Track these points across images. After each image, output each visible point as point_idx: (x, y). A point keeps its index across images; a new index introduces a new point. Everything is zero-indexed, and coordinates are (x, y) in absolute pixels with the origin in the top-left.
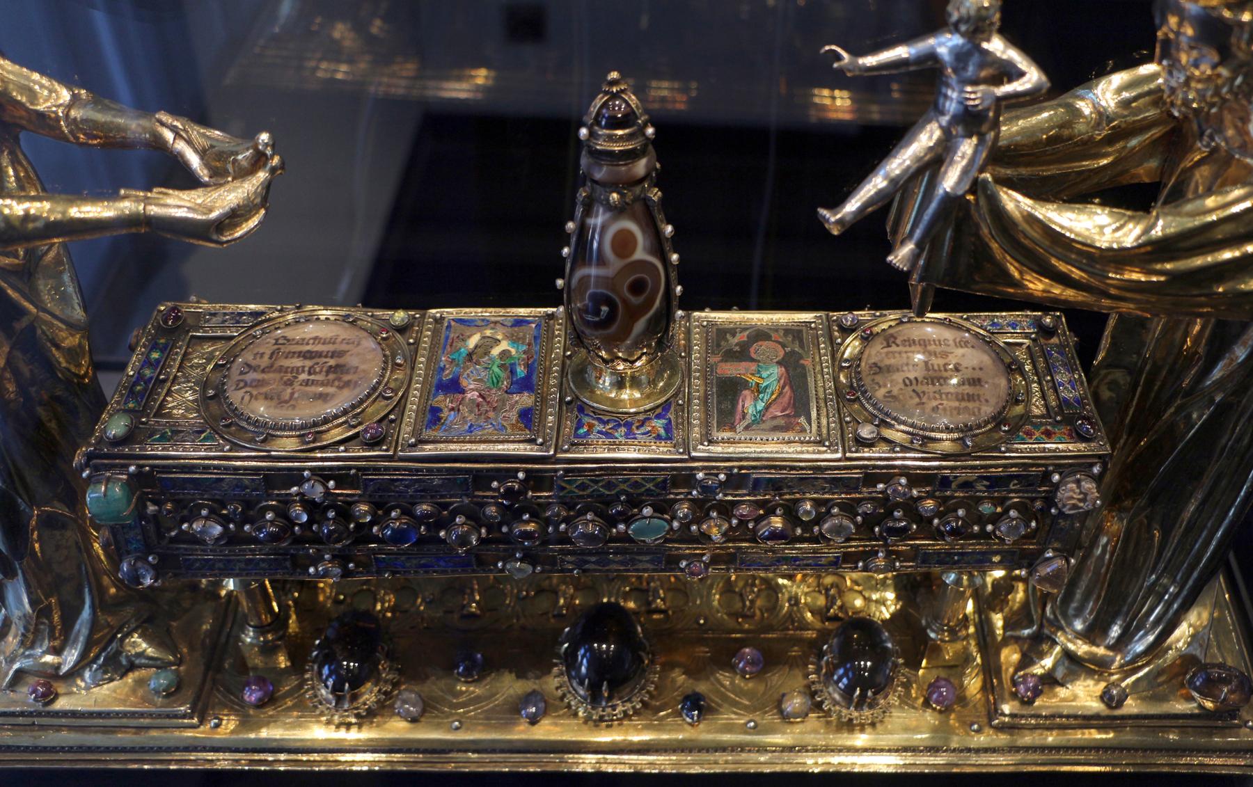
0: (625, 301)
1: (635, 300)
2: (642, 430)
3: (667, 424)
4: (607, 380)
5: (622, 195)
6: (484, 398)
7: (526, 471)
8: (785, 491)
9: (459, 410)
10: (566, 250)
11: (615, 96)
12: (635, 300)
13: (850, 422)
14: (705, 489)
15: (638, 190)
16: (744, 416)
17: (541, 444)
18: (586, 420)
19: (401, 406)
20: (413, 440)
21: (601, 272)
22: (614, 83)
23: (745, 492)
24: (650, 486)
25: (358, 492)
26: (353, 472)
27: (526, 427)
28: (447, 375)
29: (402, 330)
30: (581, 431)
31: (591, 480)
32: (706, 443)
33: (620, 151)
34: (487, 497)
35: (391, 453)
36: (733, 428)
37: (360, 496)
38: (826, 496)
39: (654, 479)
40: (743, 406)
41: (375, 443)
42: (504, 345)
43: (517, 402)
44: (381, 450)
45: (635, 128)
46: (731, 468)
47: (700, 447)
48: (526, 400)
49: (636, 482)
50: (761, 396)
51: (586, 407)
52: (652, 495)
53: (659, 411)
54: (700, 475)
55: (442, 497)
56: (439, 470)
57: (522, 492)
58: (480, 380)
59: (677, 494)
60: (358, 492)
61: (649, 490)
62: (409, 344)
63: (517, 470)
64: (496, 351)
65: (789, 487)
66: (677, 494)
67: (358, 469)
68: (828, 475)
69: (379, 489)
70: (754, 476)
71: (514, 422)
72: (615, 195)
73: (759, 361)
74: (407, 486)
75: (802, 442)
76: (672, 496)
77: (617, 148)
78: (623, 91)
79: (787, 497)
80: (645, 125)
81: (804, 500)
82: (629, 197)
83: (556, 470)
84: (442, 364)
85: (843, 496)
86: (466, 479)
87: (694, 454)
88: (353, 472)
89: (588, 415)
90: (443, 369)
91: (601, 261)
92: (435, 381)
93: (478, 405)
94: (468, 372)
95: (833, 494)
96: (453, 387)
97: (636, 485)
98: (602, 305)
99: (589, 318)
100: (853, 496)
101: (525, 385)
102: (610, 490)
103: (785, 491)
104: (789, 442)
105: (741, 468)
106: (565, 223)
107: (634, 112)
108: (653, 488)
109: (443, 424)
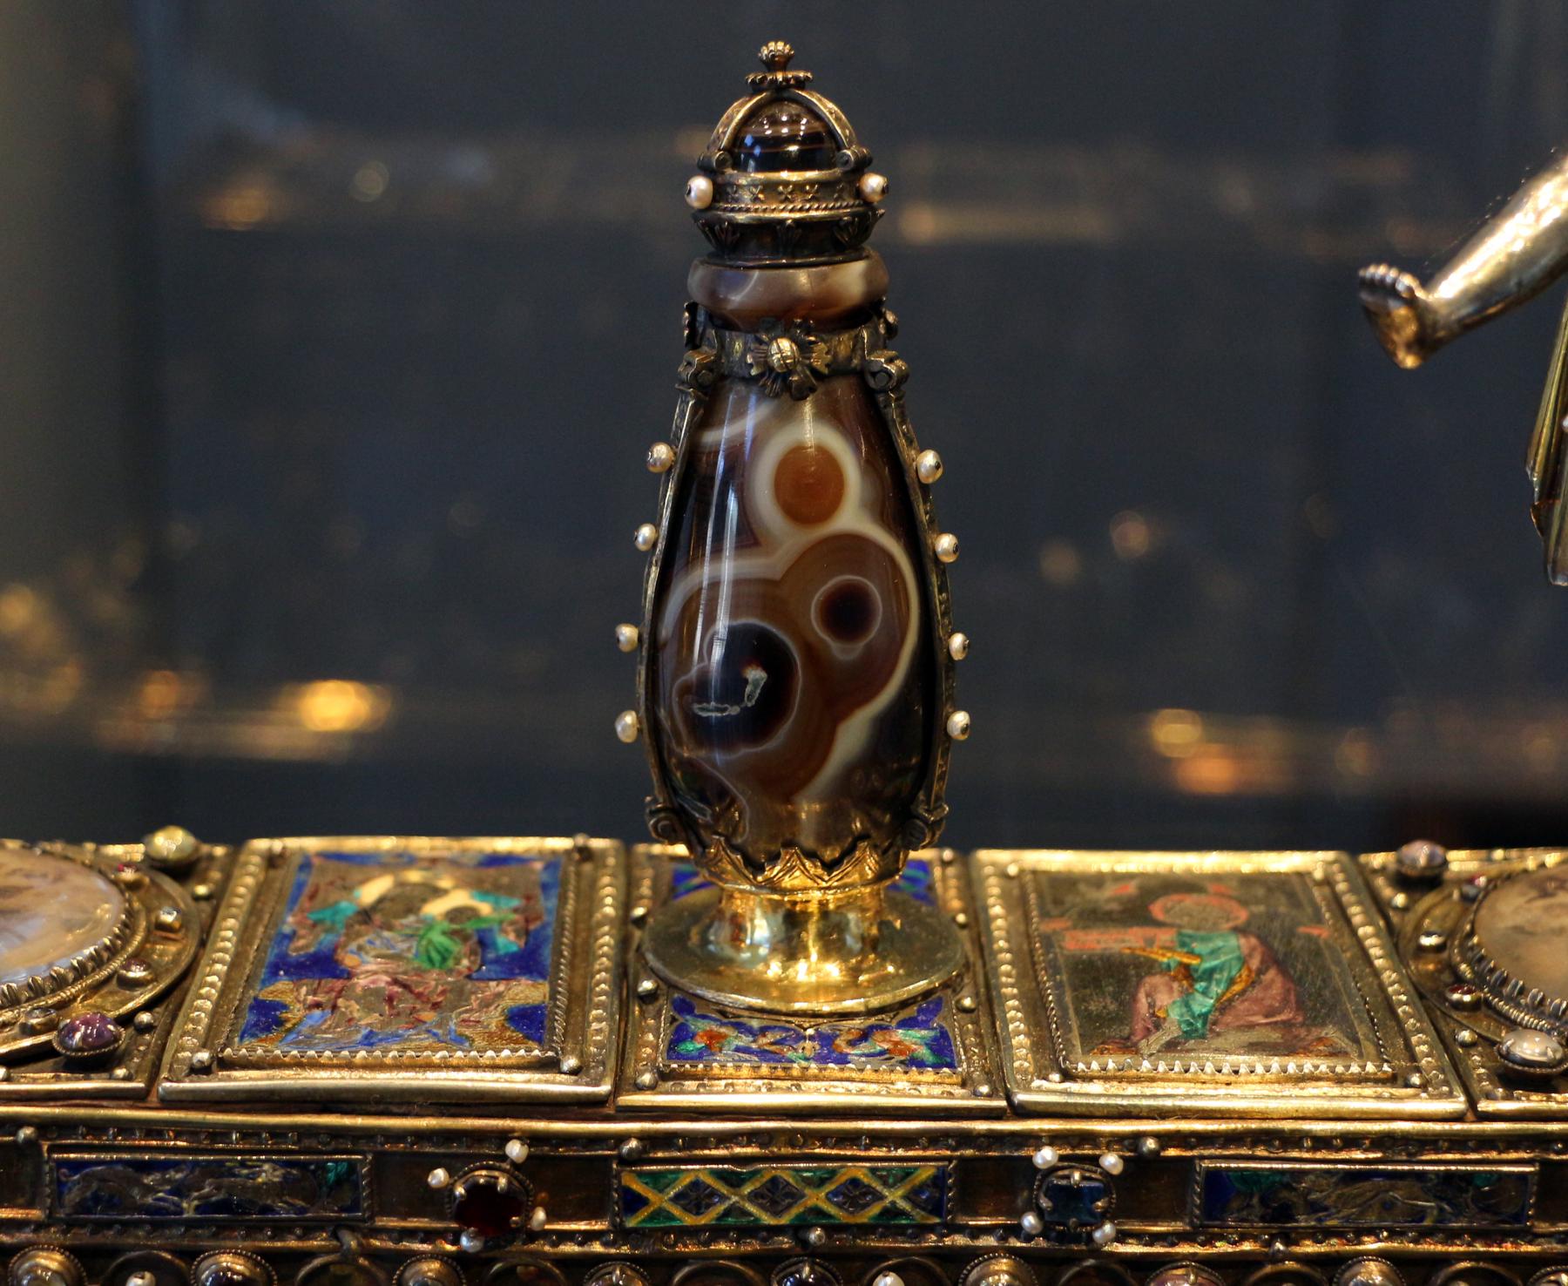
0: (812, 653)
1: (841, 652)
2: (864, 1048)
3: (935, 1039)
4: (761, 929)
5: (804, 348)
6: (405, 986)
7: (531, 1139)
8: (1303, 1221)
9: (334, 1007)
10: (646, 532)
11: (781, 94)
12: (841, 652)
13: (1473, 1045)
14: (1068, 1198)
15: (843, 343)
16: (1158, 1024)
17: (574, 1072)
18: (700, 1026)
19: (172, 997)
20: (204, 1056)
21: (756, 565)
22: (773, 64)
23: (1178, 1226)
24: (895, 1196)
25: (36, 1214)
26: (25, 1133)
27: (527, 1037)
28: (297, 950)
29: (182, 870)
30: (689, 1047)
31: (720, 1175)
32: (1056, 1077)
33: (796, 221)
34: (411, 1234)
35: (138, 1084)
36: (1128, 1046)
37: (39, 1226)
38: (1428, 1247)
39: (907, 1174)
40: (1151, 1006)
41: (97, 1060)
42: (460, 898)
43: (499, 995)
44: (111, 1078)
45: (838, 171)
46: (1138, 1137)
47: (1037, 1083)
48: (527, 992)
49: (855, 1182)
50: (1200, 986)
51: (695, 1002)
52: (900, 1231)
53: (912, 1011)
54: (1046, 1156)
55: (281, 1230)
56: (277, 1132)
57: (515, 1202)
58: (397, 957)
59: (977, 1232)
60: (36, 1214)
61: (892, 1212)
62: (197, 898)
63: (504, 1136)
64: (435, 908)
65: (1314, 1208)
66: (977, 1232)
67: (44, 1126)
68: (1432, 1163)
69: (96, 1199)
70: (1206, 1164)
71: (493, 1027)
72: (785, 345)
73: (1180, 927)
74: (180, 1190)
75: (1340, 1080)
76: (960, 1240)
77: (786, 214)
78: (801, 84)
79: (1309, 1247)
80: (862, 167)
81: (1359, 1257)
82: (819, 359)
83: (623, 1138)
84: (287, 929)
85: (1480, 1248)
86: (352, 1165)
87: (1021, 1097)
88: (25, 1133)
89: (704, 1017)
90: (292, 936)
91: (750, 537)
92: (270, 956)
93: (390, 999)
94: (362, 941)
95: (1452, 1236)
96: (324, 966)
97: (855, 1194)
98: (749, 663)
99: (711, 712)
100: (1508, 1247)
101: (526, 963)
102: (776, 1213)
103: (1303, 1221)
104: (1301, 1079)
105: (1165, 1139)
106: (649, 447)
107: (831, 133)
108: (903, 1205)
109: (289, 1031)
